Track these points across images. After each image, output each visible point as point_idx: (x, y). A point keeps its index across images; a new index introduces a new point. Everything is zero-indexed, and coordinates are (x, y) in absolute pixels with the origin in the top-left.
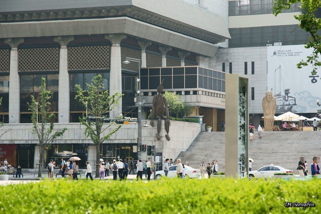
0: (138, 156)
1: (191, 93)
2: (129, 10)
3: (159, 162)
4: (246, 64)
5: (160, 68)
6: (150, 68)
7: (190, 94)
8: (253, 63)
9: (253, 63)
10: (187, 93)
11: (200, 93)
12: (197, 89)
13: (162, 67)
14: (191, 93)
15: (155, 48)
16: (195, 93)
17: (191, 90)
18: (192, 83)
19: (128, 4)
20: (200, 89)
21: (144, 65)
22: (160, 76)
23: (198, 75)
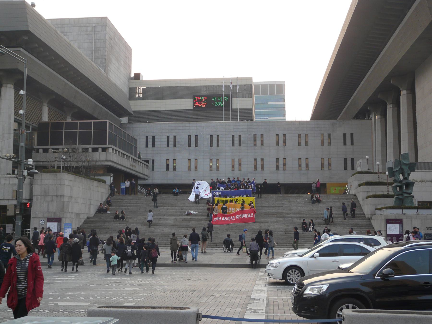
0: (16, 222)
1: (100, 150)
2: (26, 38)
3: (56, 231)
4: (147, 137)
5: (64, 122)
6: (53, 122)
7: (98, 152)
8: (154, 137)
9: (154, 137)
10: (95, 150)
11: (110, 150)
12: (107, 145)
13: (66, 121)
14: (100, 150)
15: (59, 103)
16: (104, 150)
17: (100, 146)
18: (100, 138)
19: (25, 29)
20: (110, 146)
21: (45, 119)
22: (64, 131)
23: (108, 130)
